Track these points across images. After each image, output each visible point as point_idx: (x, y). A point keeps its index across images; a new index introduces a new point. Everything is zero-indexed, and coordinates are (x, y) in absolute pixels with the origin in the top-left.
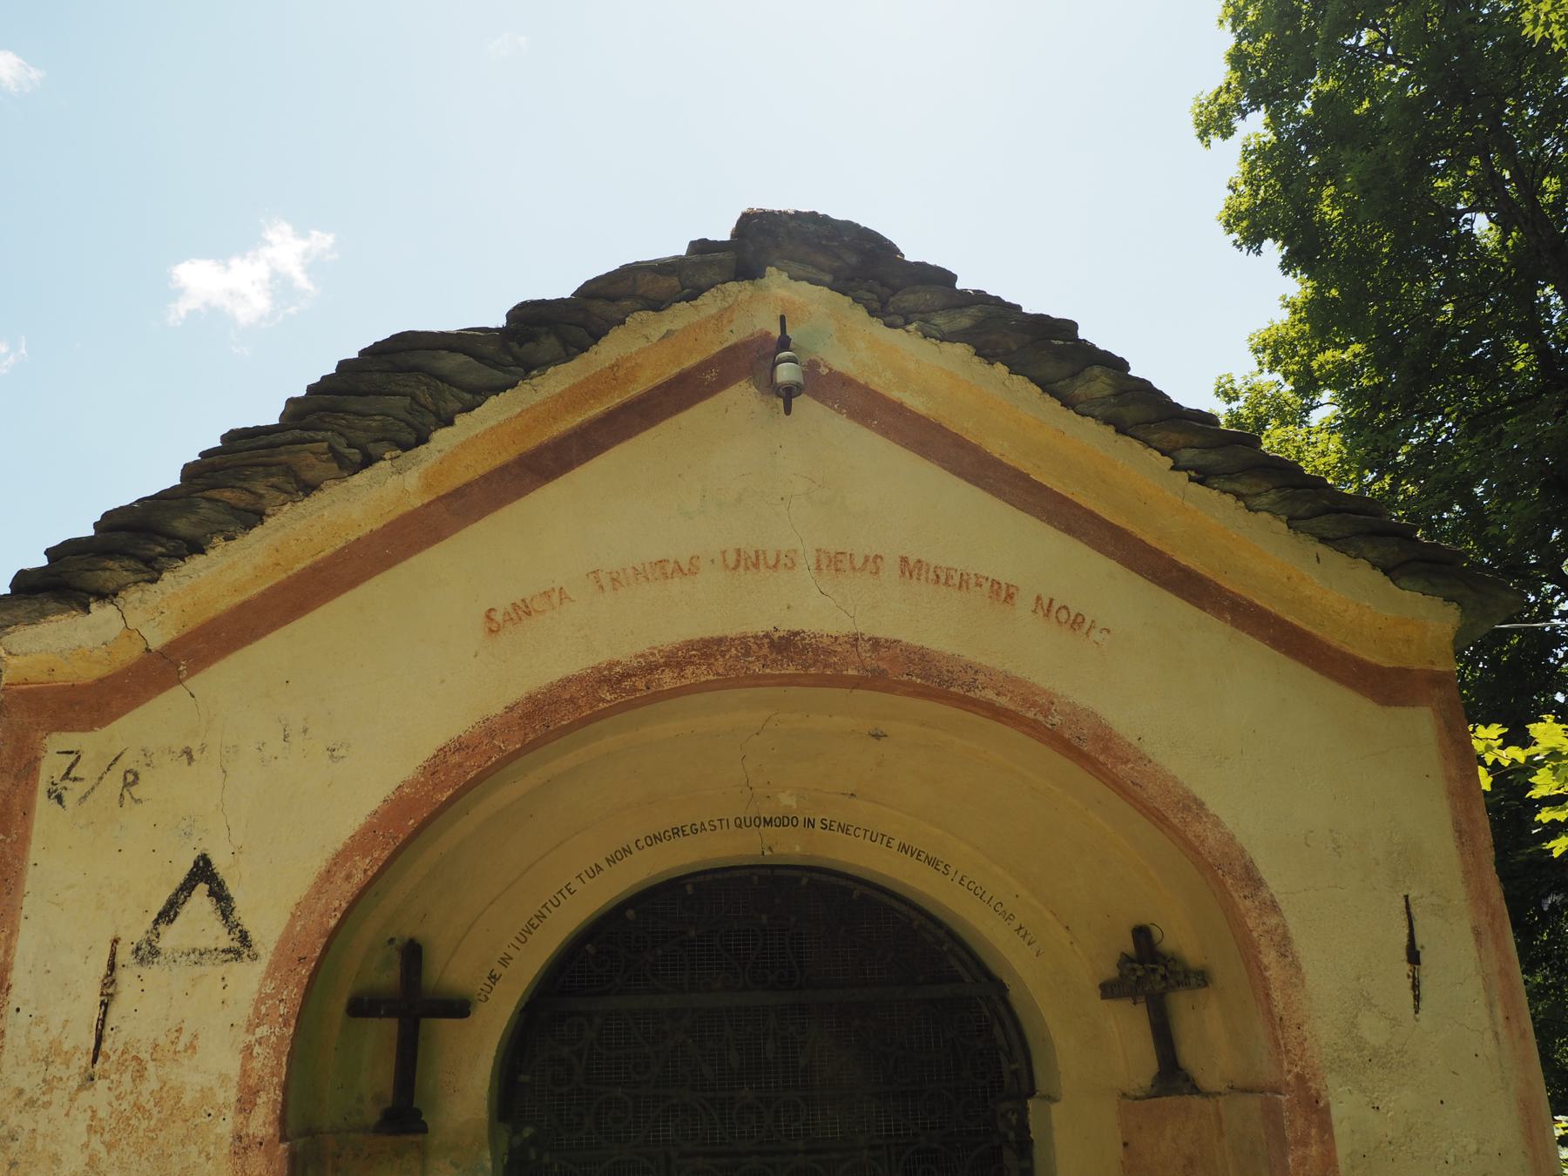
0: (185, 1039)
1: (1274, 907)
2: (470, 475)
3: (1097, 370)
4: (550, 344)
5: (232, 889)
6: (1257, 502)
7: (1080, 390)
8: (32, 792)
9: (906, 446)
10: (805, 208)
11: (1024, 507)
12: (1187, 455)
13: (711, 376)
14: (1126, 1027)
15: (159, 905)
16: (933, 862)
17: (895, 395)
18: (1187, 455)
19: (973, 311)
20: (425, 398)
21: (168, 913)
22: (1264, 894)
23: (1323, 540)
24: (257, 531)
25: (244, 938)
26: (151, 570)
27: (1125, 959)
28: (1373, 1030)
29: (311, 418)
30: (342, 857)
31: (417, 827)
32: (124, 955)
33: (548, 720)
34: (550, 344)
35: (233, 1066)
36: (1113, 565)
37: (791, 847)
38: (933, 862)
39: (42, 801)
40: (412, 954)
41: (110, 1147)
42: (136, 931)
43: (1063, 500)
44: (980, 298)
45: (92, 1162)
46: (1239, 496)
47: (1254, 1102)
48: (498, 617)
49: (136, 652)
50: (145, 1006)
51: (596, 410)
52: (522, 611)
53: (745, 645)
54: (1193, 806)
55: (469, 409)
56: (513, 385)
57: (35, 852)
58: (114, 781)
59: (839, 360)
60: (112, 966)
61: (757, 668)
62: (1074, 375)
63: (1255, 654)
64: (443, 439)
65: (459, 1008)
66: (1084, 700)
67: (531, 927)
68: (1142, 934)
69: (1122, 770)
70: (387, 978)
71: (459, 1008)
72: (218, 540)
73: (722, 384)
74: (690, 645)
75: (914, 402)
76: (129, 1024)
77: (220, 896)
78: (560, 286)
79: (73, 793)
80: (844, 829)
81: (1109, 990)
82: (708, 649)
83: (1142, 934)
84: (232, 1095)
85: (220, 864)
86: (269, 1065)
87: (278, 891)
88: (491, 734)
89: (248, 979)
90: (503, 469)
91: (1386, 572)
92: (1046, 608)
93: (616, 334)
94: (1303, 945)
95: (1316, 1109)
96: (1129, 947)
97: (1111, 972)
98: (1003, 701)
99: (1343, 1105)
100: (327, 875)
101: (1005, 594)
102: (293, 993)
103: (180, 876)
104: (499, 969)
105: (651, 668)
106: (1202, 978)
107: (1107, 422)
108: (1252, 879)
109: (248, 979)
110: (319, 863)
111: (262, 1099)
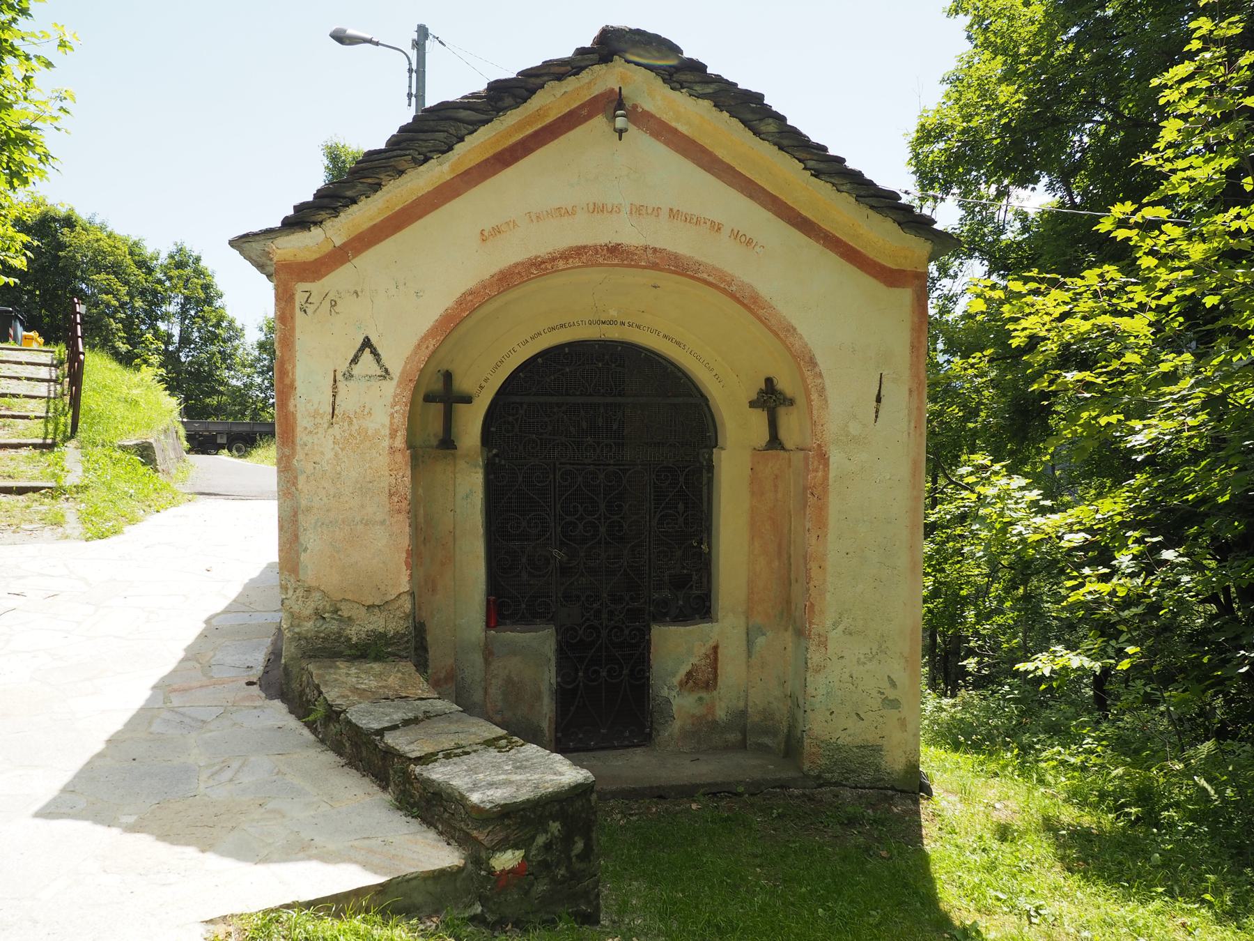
0: (367, 410)
1: (820, 375)
2: (472, 164)
3: (770, 120)
4: (508, 101)
5: (380, 351)
6: (842, 188)
7: (763, 128)
8: (293, 308)
9: (677, 151)
10: (634, 26)
11: (731, 185)
12: (811, 164)
13: (584, 112)
14: (759, 420)
15: (351, 357)
16: (678, 343)
17: (674, 124)
18: (811, 164)
19: (713, 86)
20: (452, 131)
21: (355, 360)
22: (817, 370)
23: (872, 207)
24: (379, 193)
25: (386, 371)
26: (336, 212)
27: (761, 391)
28: (854, 429)
29: (404, 145)
30: (424, 339)
31: (452, 325)
32: (339, 377)
33: (507, 280)
34: (508, 101)
35: (387, 421)
36: (769, 215)
37: (613, 333)
38: (678, 343)
39: (298, 313)
40: (448, 377)
41: (342, 450)
42: (343, 367)
43: (750, 181)
44: (718, 79)
45: (336, 455)
46: (834, 185)
47: (801, 454)
48: (486, 233)
49: (330, 247)
50: (350, 397)
51: (530, 131)
52: (497, 231)
53: (596, 249)
54: (791, 330)
55: (471, 133)
56: (491, 120)
57: (298, 333)
58: (327, 304)
59: (647, 105)
60: (335, 381)
61: (601, 260)
62: (760, 120)
63: (832, 260)
64: (459, 148)
65: (467, 399)
66: (746, 280)
67: (497, 366)
68: (769, 381)
69: (761, 312)
70: (438, 386)
71: (467, 399)
72: (363, 198)
73: (590, 116)
74: (571, 249)
75: (683, 128)
76: (344, 403)
77: (375, 353)
78: (510, 73)
79: (310, 309)
80: (638, 327)
81: (753, 404)
82: (579, 251)
83: (769, 381)
84: (388, 432)
85: (374, 341)
86: (401, 421)
87: (400, 351)
88: (485, 287)
89: (390, 387)
90: (487, 160)
91: (899, 224)
92: (736, 235)
93: (540, 93)
94: (831, 393)
95: (823, 458)
96: (763, 387)
97: (754, 396)
98: (711, 279)
99: (836, 457)
100: (419, 346)
101: (717, 228)
102: (408, 393)
103: (358, 346)
104: (484, 384)
105: (554, 259)
106: (791, 402)
107: (775, 144)
108: (812, 363)
109: (390, 387)
110: (415, 341)
111: (399, 434)
